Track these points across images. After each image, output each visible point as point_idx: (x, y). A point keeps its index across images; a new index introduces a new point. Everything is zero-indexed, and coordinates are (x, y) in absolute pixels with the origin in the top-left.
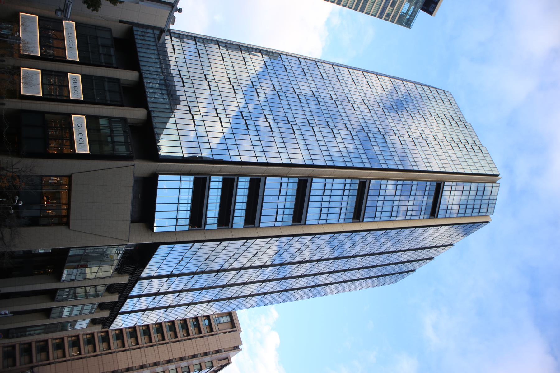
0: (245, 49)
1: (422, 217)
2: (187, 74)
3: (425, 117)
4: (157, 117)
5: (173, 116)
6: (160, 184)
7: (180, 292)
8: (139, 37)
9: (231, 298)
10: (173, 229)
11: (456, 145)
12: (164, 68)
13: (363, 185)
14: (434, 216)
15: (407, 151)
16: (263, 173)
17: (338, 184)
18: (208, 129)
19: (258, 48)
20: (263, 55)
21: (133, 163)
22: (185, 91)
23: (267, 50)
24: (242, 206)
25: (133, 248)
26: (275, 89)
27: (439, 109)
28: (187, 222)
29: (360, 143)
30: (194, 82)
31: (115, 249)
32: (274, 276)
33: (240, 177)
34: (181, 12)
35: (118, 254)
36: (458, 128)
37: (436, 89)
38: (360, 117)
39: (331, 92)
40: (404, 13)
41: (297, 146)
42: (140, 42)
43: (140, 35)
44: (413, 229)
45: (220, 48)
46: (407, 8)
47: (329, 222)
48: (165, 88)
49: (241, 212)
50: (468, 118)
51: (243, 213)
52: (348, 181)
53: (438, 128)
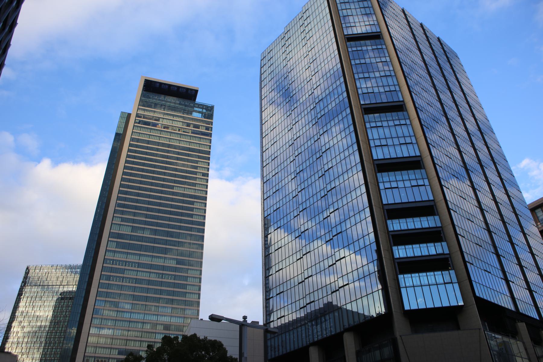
0: (267, 251)
1: (384, 47)
2: (301, 301)
3: (289, 70)
4: (348, 322)
5: (345, 307)
6: (414, 307)
7: (521, 267)
8: (277, 353)
9: (502, 220)
10: (456, 286)
11: (308, 35)
12: (301, 323)
13: (368, 110)
14: (379, 35)
15: (328, 75)
16: (380, 208)
17: (373, 134)
18: (349, 270)
19: (263, 239)
20: (269, 233)
21: (398, 338)
22: (323, 298)
23: (263, 230)
24: (417, 221)
25: (486, 323)
26: (298, 215)
27: (279, 60)
28: (446, 273)
29: (333, 120)
30: (307, 293)
31: (492, 342)
32: (480, 174)
33: (390, 230)
34: (247, 317)
35: (496, 338)
36: (292, 38)
37: (261, 68)
38: (307, 127)
39: (289, 162)
40: (202, 115)
41: (347, 182)
42: (281, 351)
43: (275, 352)
44: (398, 51)
45: (272, 275)
46: (197, 113)
47: (412, 134)
48: (320, 319)
49: (423, 221)
50: (281, 31)
51: (424, 219)
52: (368, 125)
53: (296, 55)
